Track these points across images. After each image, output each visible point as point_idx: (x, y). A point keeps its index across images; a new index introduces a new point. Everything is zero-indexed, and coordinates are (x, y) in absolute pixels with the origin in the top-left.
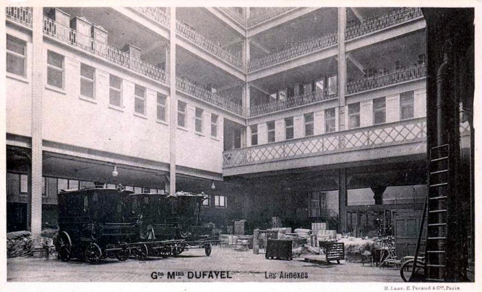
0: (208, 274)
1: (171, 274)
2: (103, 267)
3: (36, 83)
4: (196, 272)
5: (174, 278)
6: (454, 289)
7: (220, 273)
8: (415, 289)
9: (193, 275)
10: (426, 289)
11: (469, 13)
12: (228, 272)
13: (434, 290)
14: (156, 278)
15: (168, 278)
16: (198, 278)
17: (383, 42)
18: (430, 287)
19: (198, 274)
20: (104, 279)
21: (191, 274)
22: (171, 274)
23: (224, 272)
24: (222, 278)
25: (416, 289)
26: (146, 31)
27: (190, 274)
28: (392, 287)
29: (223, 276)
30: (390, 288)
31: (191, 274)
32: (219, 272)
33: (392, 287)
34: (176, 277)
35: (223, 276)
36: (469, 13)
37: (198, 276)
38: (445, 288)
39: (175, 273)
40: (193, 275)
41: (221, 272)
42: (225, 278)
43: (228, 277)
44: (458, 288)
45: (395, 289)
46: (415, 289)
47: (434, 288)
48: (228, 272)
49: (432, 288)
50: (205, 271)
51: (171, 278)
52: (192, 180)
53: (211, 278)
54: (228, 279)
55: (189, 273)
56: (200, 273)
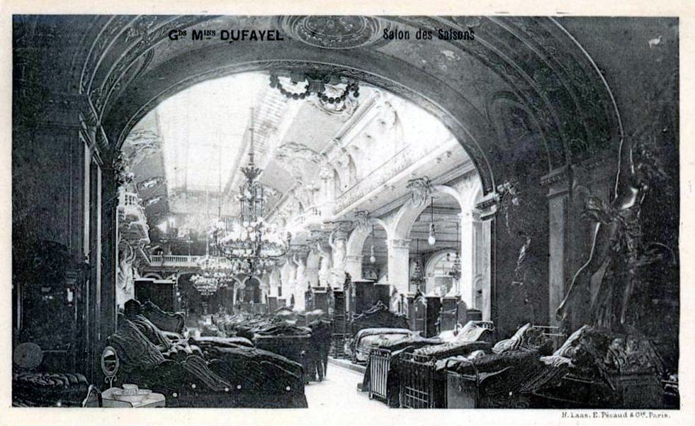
4: (232, 31)
5: (201, 39)
7: (266, 32)
8: (605, 416)
9: (228, 35)
11: (25, 393)
12: (572, 417)
14: (176, 39)
15: (193, 39)
16: (226, 39)
17: (96, 274)
19: (235, 35)
21: (225, 34)
24: (269, 39)
25: (607, 416)
27: (226, 37)
29: (272, 37)
36: (25, 393)
39: (203, 32)
40: (228, 35)
41: (269, 31)
42: (273, 39)
43: (278, 39)
44: (666, 416)
46: (605, 416)
47: (632, 415)
48: (572, 417)
52: (197, 71)
56: (239, 31)
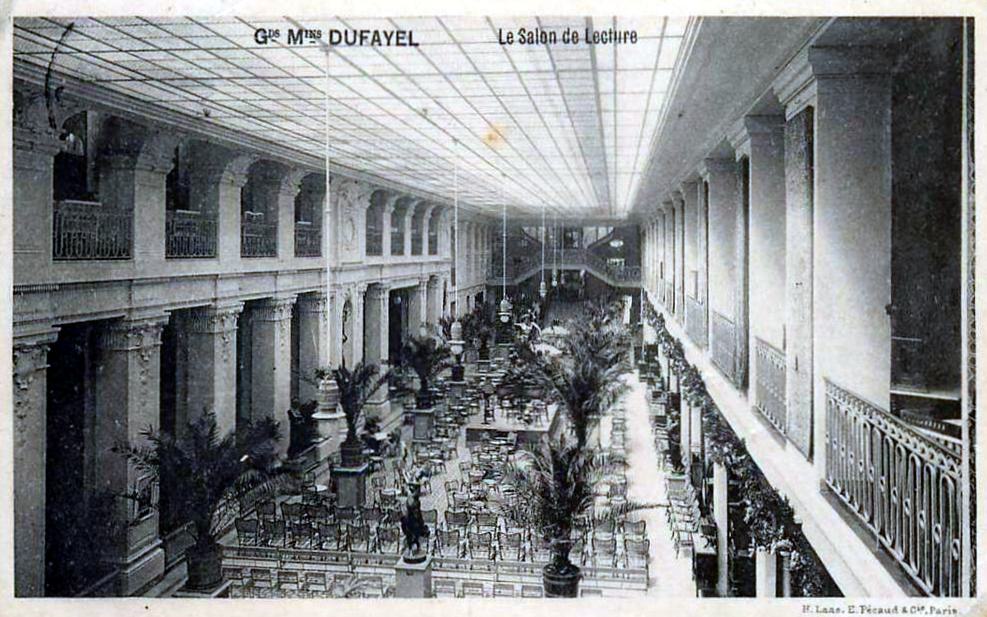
0: (370, 36)
1: (295, 33)
2: (46, 217)
3: (923, 451)
5: (301, 42)
6: (947, 613)
9: (340, 37)
10: (889, 612)
13: (905, 615)
18: (896, 609)
20: (18, 462)
22: (295, 33)
23: (404, 32)
24: (398, 44)
25: (869, 611)
26: (525, 377)
28: (817, 607)
29: (401, 41)
30: (815, 610)
31: (336, 37)
32: (392, 33)
33: (817, 607)
34: (306, 41)
35: (401, 41)
37: (351, 39)
38: (928, 609)
40: (340, 37)
42: (404, 45)
43: (411, 44)
45: (825, 611)
46: (865, 611)
47: (904, 611)
49: (900, 609)
50: (364, 29)
51: (295, 40)
53: (376, 43)
54: (413, 47)
55: (331, 32)
